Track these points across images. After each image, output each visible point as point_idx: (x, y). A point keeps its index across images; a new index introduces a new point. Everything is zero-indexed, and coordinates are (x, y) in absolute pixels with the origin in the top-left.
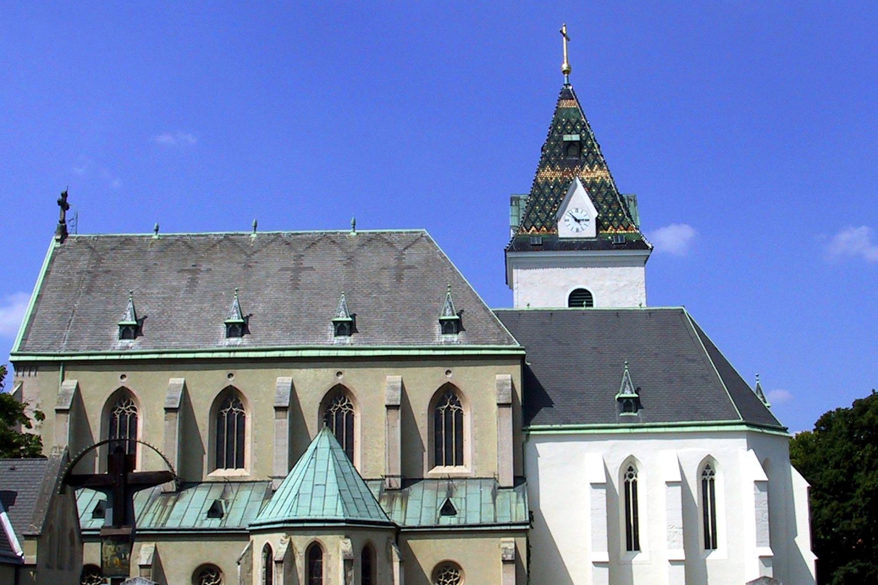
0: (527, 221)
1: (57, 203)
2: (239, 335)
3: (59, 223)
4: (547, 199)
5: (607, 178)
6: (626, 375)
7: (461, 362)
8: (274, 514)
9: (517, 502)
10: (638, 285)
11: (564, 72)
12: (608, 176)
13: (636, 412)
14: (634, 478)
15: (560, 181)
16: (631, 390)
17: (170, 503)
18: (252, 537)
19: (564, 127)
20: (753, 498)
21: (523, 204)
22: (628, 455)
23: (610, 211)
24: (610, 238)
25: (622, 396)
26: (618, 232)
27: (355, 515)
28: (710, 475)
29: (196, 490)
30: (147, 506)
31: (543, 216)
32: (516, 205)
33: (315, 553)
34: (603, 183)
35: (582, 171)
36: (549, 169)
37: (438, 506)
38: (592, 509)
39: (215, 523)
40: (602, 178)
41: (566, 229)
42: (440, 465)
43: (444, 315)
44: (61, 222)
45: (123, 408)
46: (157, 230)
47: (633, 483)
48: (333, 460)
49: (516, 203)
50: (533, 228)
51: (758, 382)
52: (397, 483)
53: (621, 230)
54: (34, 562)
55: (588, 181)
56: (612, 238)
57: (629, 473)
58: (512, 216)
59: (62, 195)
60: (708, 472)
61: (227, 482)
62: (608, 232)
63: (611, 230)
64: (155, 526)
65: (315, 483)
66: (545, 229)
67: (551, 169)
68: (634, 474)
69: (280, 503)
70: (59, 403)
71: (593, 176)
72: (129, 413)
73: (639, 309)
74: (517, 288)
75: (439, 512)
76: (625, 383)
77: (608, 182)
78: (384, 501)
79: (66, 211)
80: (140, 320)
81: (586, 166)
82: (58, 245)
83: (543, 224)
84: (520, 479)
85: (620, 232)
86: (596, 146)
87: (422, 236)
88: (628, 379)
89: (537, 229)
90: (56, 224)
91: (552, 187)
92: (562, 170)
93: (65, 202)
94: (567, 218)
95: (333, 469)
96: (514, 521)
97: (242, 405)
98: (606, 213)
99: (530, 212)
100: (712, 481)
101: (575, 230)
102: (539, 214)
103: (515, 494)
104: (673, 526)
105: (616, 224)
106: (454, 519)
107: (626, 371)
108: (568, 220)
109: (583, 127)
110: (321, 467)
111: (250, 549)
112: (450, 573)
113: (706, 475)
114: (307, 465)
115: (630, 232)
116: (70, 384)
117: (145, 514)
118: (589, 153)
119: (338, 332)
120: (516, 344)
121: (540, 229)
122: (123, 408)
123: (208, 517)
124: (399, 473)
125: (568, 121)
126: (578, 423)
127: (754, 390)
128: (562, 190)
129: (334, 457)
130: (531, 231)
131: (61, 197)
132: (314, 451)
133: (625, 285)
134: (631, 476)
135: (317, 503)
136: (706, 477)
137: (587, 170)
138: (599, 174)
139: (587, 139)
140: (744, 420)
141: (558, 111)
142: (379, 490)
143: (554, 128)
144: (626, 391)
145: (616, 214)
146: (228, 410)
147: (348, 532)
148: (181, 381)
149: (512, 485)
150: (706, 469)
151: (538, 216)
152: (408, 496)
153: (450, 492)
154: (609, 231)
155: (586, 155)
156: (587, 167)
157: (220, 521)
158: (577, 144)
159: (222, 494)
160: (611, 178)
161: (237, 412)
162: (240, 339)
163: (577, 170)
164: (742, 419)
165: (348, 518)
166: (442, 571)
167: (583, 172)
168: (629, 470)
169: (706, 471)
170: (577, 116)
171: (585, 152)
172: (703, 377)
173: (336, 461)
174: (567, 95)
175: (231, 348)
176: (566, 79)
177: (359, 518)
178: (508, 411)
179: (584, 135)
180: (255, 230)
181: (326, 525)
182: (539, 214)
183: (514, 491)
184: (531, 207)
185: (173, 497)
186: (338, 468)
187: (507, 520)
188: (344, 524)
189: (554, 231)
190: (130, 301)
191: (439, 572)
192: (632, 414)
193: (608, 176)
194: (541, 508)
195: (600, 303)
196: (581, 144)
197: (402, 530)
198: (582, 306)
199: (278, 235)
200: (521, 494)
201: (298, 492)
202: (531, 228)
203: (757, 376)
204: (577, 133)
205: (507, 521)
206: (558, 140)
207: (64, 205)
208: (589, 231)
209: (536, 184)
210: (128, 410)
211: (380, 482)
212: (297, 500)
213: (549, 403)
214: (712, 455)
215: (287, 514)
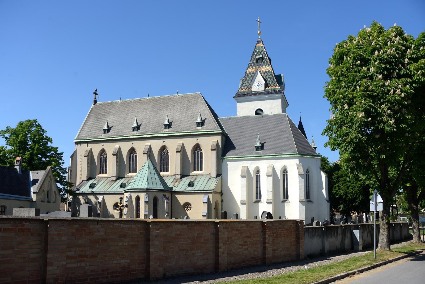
7: (201, 136)
9: (214, 183)
11: (259, 34)
14: (259, 174)
19: (257, 53)
20: (298, 180)
22: (256, 166)
23: (271, 81)
24: (269, 90)
31: (248, 84)
35: (262, 67)
38: (241, 185)
41: (255, 88)
42: (165, 172)
44: (95, 99)
45: (104, 155)
46: (121, 99)
47: (259, 176)
50: (244, 89)
52: (179, 177)
53: (274, 87)
54: (35, 200)
60: (285, 171)
62: (269, 88)
63: (270, 88)
66: (248, 89)
70: (84, 155)
72: (166, 153)
74: (238, 110)
79: (97, 95)
80: (203, 120)
82: (93, 106)
83: (247, 87)
84: (219, 175)
97: (136, 153)
98: (269, 82)
100: (287, 175)
105: (272, 85)
110: (144, 172)
112: (188, 206)
116: (89, 148)
120: (219, 129)
122: (104, 155)
125: (259, 51)
126: (240, 155)
128: (254, 75)
130: (243, 90)
133: (275, 106)
134: (258, 173)
136: (284, 173)
137: (264, 67)
139: (265, 56)
143: (254, 54)
145: (272, 82)
146: (197, 151)
147: (148, 193)
148: (119, 146)
149: (215, 177)
151: (246, 85)
154: (269, 88)
156: (264, 66)
158: (261, 58)
161: (200, 152)
163: (261, 68)
165: (148, 188)
166: (186, 206)
168: (257, 171)
169: (285, 171)
170: (262, 49)
172: (287, 138)
174: (259, 42)
176: (259, 36)
177: (153, 188)
178: (214, 152)
186: (149, 172)
188: (146, 190)
189: (251, 89)
191: (185, 206)
194: (229, 185)
197: (173, 192)
202: (243, 89)
203: (313, 136)
206: (255, 58)
208: (262, 88)
210: (166, 152)
213: (234, 148)
214: (286, 165)
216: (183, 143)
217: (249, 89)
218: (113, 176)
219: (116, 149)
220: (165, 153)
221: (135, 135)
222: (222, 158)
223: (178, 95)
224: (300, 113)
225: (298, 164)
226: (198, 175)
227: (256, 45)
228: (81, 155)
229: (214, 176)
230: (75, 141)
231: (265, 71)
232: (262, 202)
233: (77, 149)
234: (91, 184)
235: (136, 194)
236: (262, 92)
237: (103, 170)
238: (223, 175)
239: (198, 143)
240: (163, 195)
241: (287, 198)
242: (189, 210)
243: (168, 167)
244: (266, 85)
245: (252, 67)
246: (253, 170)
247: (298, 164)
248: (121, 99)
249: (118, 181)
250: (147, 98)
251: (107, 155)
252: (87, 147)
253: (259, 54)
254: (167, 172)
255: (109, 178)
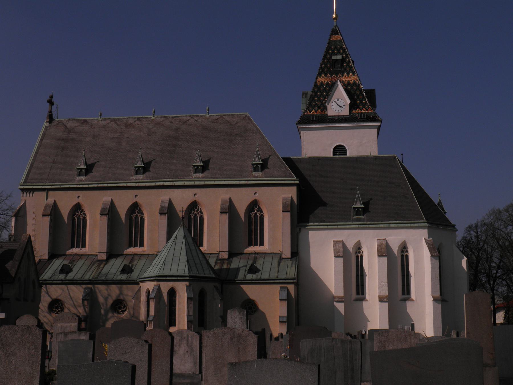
0: (309, 106)
1: (47, 102)
2: (142, 173)
3: (48, 113)
4: (322, 94)
5: (357, 80)
6: (358, 194)
8: (151, 273)
9: (292, 266)
10: (373, 142)
11: (334, 19)
12: (358, 79)
13: (363, 215)
15: (329, 83)
16: (360, 203)
17: (102, 266)
18: (141, 284)
21: (309, 96)
22: (357, 240)
25: (355, 206)
26: (362, 112)
27: (195, 273)
28: (406, 252)
29: (117, 259)
30: (90, 267)
31: (319, 104)
32: (305, 97)
33: (172, 293)
34: (355, 83)
35: (343, 76)
36: (324, 76)
37: (247, 269)
39: (124, 277)
40: (354, 80)
43: (254, 161)
46: (101, 116)
47: (360, 256)
48: (185, 243)
49: (305, 96)
51: (440, 198)
53: (364, 111)
55: (346, 82)
56: (359, 115)
57: (359, 250)
58: (303, 104)
59: (50, 97)
60: (405, 250)
61: (134, 255)
63: (358, 111)
64: (58, 278)
65: (174, 255)
66: (320, 111)
67: (325, 76)
68: (361, 252)
69: (156, 266)
71: (349, 80)
72: (82, 217)
73: (370, 156)
75: (247, 272)
76: (357, 199)
77: (357, 83)
78: (218, 265)
81: (345, 74)
82: (48, 124)
84: (295, 254)
85: (363, 112)
86: (351, 62)
87: (246, 117)
88: (359, 197)
89: (315, 111)
90: (46, 113)
91: (325, 86)
92: (331, 76)
93: (52, 101)
94: (332, 104)
95: (185, 248)
96: (288, 277)
99: (312, 101)
101: (337, 111)
102: (317, 102)
103: (291, 262)
104: (382, 282)
106: (255, 275)
107: (358, 192)
108: (333, 106)
109: (344, 51)
111: (139, 290)
113: (404, 252)
114: (171, 245)
115: (369, 111)
116: (51, 201)
117: (88, 272)
118: (347, 66)
119: (195, 171)
120: (294, 177)
121: (317, 111)
123: (121, 274)
124: (227, 250)
125: (335, 48)
126: (329, 222)
127: (436, 204)
128: (332, 86)
129: (186, 241)
130: (312, 112)
131: (49, 98)
132: (175, 237)
135: (175, 266)
137: (345, 76)
138: (352, 78)
140: (426, 220)
141: (330, 42)
142: (216, 259)
143: (327, 52)
144: (357, 204)
146: (254, 213)
148: (110, 199)
150: (404, 249)
151: (316, 103)
152: (231, 263)
153: (255, 261)
154: (357, 111)
155: (345, 67)
156: (345, 74)
157: (127, 276)
159: (130, 261)
160: (360, 80)
162: (142, 176)
163: (340, 76)
164: (425, 220)
165: (191, 274)
167: (343, 77)
169: (404, 250)
171: (345, 66)
173: (187, 243)
174: (335, 32)
175: (137, 181)
179: (344, 55)
180: (154, 115)
181: (179, 278)
182: (317, 102)
183: (291, 260)
184: (312, 98)
185: (104, 263)
187: (284, 277)
189: (325, 112)
190: (83, 155)
192: (361, 217)
193: (358, 79)
195: (351, 152)
196: (343, 60)
197: (237, 282)
198: (337, 155)
199: (166, 117)
200: (294, 262)
201: (165, 260)
203: (440, 194)
204: (340, 55)
205: (284, 277)
207: (51, 102)
208: (345, 112)
209: (316, 85)
210: (82, 215)
211: (217, 255)
212: (164, 264)
214: (407, 241)
215: (158, 272)
216: (230, 198)
217: (322, 111)
218: (102, 252)
219: (104, 204)
220: (79, 216)
221: (141, 181)
222: (299, 226)
223: (208, 115)
224: (402, 154)
225: (427, 238)
226: (257, 253)
227: (330, 38)
228: (34, 213)
229: (289, 256)
230: (22, 187)
231: (348, 82)
232: (367, 300)
233: (25, 203)
234: (124, 266)
235: (171, 284)
236: (345, 117)
237: (78, 241)
238: (302, 254)
239: (256, 199)
240: (215, 286)
241: (409, 293)
242: (59, 311)
243: (85, 240)
244: (352, 106)
245: (326, 75)
246: (352, 247)
247: (427, 238)
248: (101, 116)
249: (112, 261)
250: (151, 117)
251: (85, 214)
252: (47, 198)
253: (336, 54)
254: (135, 248)
255: (91, 256)
